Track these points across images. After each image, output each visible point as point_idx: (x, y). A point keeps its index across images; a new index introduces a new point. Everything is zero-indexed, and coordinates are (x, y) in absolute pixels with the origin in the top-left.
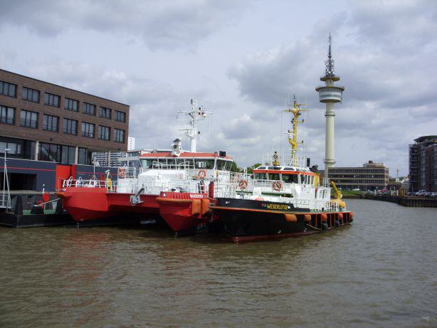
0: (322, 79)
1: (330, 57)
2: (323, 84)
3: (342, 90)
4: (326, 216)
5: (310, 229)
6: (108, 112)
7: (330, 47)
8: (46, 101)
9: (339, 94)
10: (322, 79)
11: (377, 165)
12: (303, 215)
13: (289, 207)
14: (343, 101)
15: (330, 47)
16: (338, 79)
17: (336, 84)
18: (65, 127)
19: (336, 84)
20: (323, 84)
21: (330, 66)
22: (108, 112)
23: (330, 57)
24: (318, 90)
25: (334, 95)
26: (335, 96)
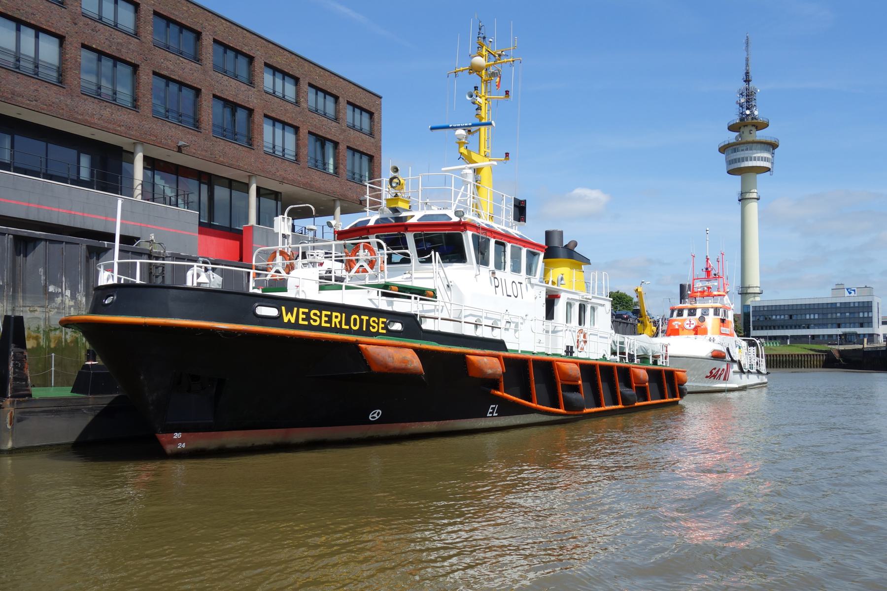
0: (732, 128)
1: (747, 81)
2: (732, 137)
3: (772, 146)
4: (574, 370)
5: (507, 408)
6: (241, 115)
7: (747, 60)
8: (89, 79)
9: (767, 155)
10: (732, 128)
11: (391, 364)
12: (463, 356)
13: (397, 327)
14: (775, 170)
15: (747, 60)
16: (765, 125)
17: (760, 135)
18: (349, 167)
19: (760, 135)
20: (732, 137)
21: (749, 97)
22: (241, 115)
23: (747, 81)
24: (723, 149)
25: (758, 158)
26: (759, 159)
